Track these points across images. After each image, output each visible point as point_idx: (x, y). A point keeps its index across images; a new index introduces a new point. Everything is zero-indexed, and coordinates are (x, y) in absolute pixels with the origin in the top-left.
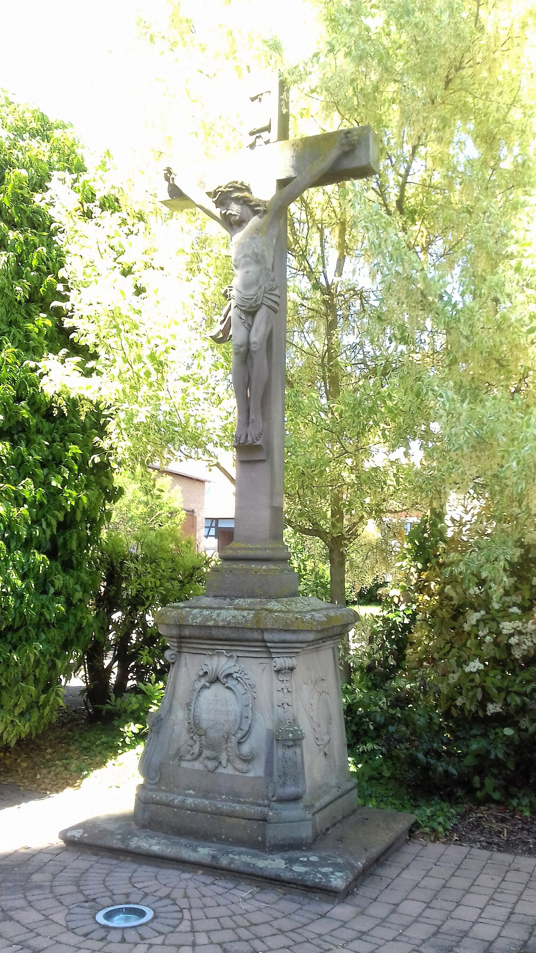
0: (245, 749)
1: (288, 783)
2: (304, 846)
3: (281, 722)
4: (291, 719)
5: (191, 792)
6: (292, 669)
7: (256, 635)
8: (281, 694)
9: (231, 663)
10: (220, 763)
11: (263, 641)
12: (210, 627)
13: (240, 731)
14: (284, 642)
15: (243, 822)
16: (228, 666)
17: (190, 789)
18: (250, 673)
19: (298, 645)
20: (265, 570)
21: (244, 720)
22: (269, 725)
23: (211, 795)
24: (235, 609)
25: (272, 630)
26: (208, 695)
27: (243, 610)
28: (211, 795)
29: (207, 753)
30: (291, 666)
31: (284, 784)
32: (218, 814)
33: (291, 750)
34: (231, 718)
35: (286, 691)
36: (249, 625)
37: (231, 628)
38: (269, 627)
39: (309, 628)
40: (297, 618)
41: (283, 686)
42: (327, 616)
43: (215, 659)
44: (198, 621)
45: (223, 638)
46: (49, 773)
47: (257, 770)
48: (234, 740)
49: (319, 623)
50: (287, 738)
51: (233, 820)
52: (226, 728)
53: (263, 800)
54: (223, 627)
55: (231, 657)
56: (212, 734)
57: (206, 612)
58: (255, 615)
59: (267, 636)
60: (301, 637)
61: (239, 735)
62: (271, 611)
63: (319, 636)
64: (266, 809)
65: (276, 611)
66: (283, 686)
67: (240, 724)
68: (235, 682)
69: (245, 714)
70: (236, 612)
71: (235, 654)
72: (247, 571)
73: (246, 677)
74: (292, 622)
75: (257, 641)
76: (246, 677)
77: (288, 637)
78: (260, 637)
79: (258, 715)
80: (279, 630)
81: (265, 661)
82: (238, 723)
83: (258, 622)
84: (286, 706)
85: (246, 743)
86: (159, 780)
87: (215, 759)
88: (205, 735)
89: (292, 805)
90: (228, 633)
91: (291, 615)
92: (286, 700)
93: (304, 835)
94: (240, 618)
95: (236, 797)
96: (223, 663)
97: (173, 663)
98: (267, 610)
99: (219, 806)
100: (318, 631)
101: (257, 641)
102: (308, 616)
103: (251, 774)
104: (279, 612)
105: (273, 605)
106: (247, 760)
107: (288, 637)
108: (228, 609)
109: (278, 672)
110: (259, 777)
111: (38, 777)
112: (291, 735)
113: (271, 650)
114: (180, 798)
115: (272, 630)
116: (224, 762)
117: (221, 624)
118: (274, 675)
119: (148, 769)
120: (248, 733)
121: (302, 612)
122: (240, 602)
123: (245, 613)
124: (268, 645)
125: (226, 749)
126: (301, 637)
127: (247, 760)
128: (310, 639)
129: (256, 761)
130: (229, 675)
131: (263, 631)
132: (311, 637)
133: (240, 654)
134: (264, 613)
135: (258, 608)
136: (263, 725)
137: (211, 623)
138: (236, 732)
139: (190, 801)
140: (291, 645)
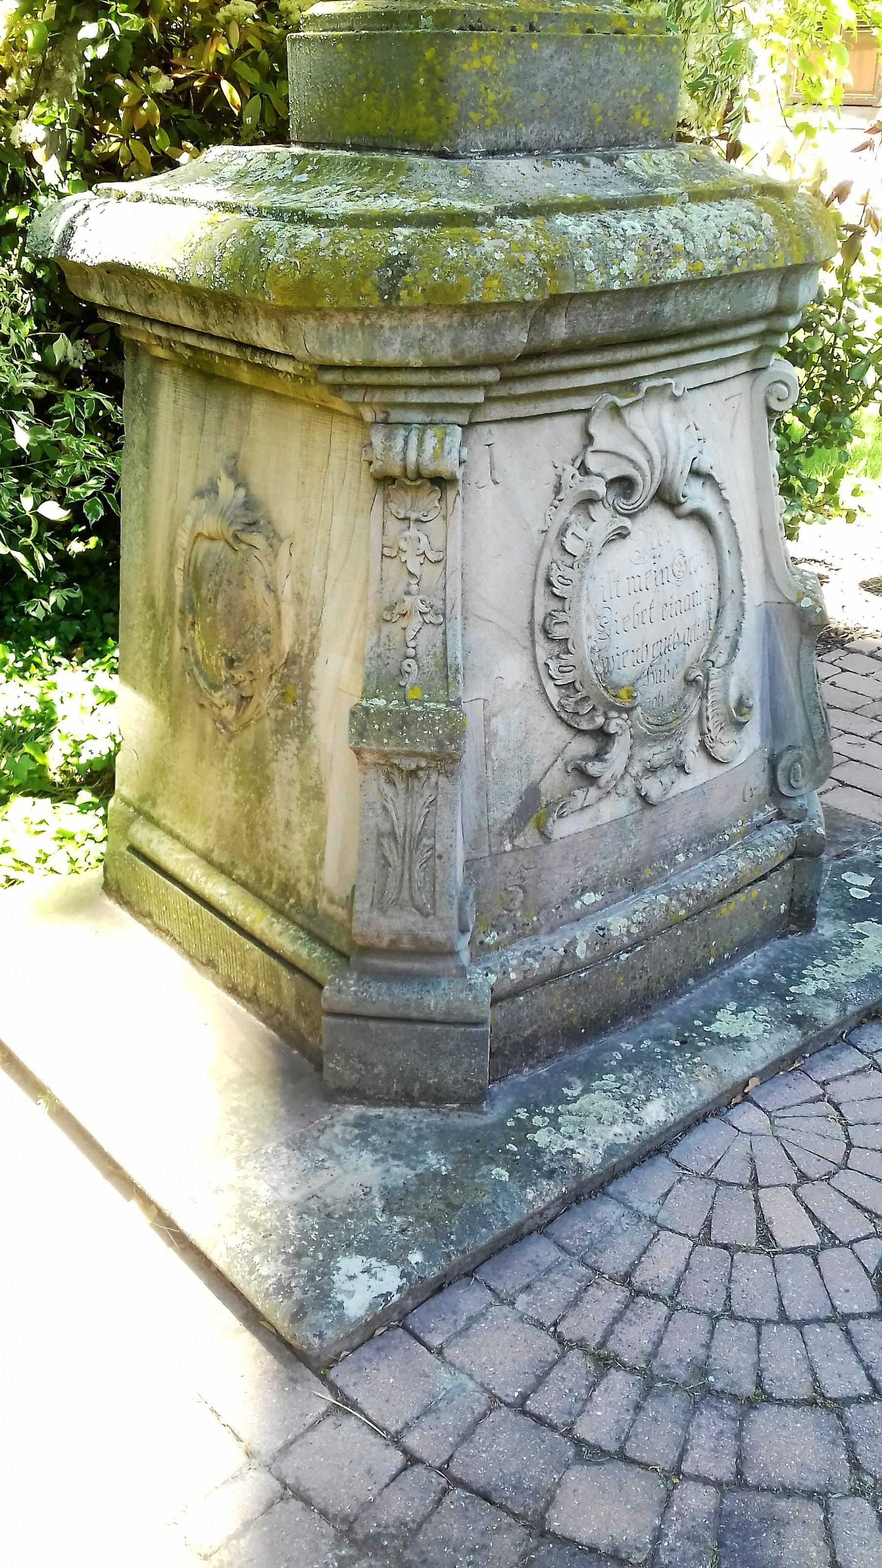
15: (755, 892)
17: (584, 890)
23: (648, 873)
28: (648, 873)
99: (700, 886)
117: (711, 267)
139: (618, 924)
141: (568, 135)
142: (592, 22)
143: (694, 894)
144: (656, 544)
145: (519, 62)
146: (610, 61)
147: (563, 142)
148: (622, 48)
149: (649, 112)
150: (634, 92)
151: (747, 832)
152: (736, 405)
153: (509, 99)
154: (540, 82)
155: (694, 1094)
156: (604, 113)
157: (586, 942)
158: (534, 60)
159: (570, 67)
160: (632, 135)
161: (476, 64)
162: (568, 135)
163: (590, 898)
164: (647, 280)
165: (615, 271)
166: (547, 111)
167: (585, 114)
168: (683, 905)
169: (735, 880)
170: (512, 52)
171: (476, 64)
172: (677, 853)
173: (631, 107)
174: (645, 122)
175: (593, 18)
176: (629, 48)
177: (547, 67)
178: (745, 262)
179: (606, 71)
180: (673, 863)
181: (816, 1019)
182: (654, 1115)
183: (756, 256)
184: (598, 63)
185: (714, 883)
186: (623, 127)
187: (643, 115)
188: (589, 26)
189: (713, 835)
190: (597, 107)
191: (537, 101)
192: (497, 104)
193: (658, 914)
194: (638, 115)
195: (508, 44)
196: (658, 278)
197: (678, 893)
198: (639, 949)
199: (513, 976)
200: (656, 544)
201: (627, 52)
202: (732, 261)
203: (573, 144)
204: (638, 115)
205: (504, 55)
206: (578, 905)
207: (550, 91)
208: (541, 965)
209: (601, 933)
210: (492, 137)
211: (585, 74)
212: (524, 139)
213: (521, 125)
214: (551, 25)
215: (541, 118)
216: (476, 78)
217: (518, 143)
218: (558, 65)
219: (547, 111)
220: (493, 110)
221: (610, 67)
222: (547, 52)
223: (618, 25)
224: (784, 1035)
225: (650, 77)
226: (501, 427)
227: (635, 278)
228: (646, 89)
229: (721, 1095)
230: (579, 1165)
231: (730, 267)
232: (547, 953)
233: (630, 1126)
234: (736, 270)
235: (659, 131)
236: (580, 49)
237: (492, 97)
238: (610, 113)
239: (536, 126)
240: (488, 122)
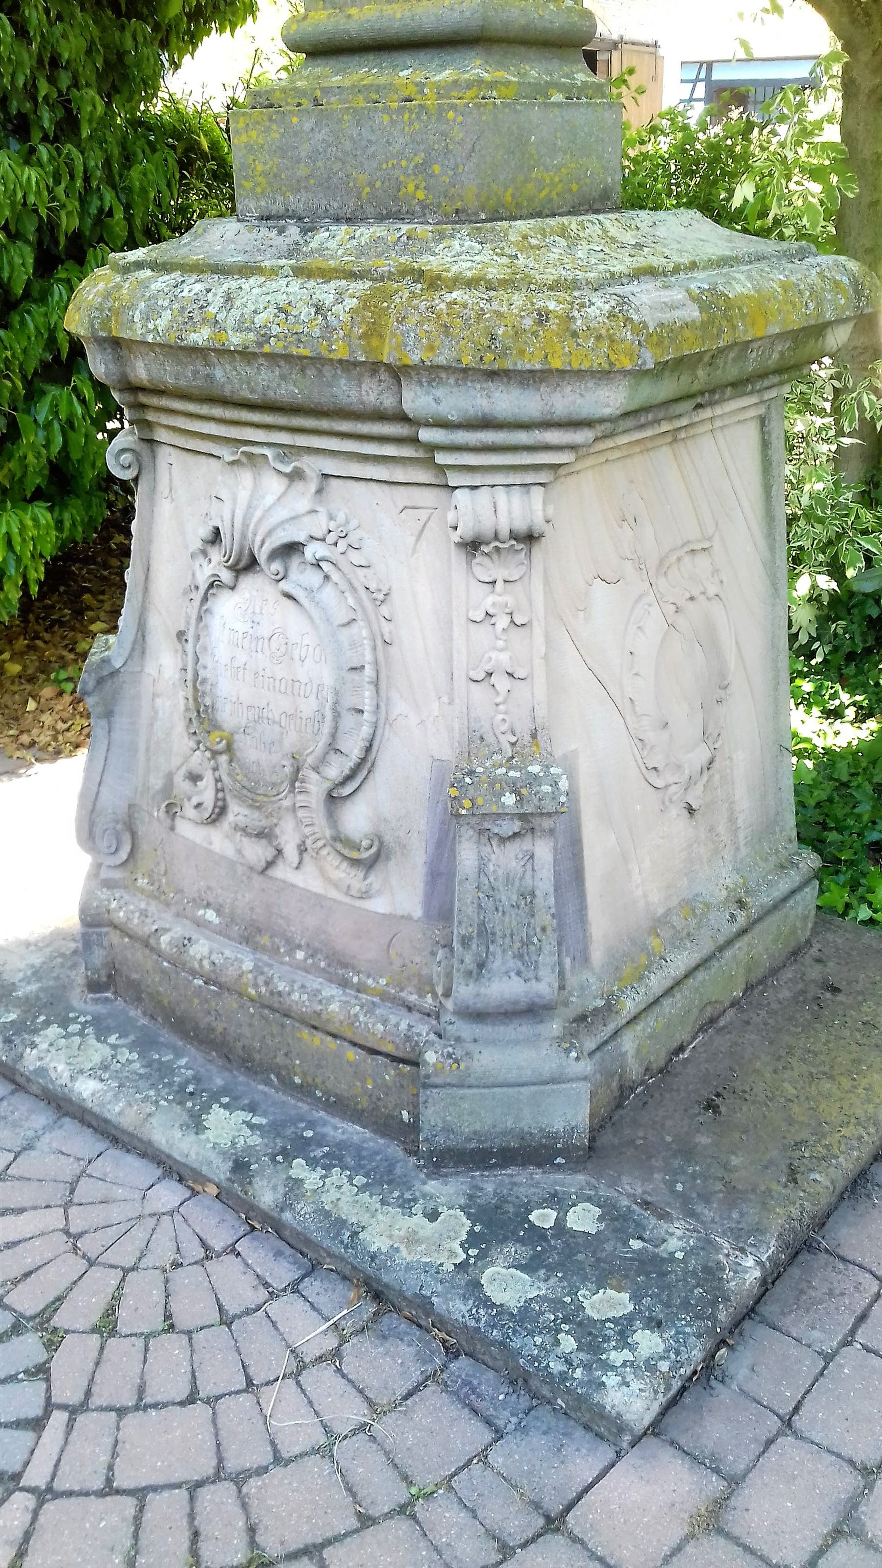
0: (357, 819)
1: (496, 964)
2: (560, 1153)
3: (475, 740)
4: (524, 730)
5: (211, 915)
6: (530, 538)
7: (372, 393)
8: (482, 634)
9: (301, 499)
10: (280, 852)
11: (403, 418)
12: (195, 351)
13: (333, 758)
14: (486, 423)
15: (352, 1054)
16: (282, 514)
17: (208, 905)
18: (370, 546)
19: (553, 437)
20: (442, 91)
21: (348, 721)
22: (443, 746)
23: (265, 940)
24: (298, 272)
25: (431, 373)
26: (228, 608)
27: (326, 275)
28: (265, 940)
29: (237, 812)
30: (521, 526)
31: (481, 966)
32: (275, 1008)
33: (514, 849)
34: (308, 707)
35: (503, 622)
36: (340, 350)
37: (272, 357)
38: (414, 358)
39: (598, 361)
40: (543, 317)
41: (489, 601)
42: (713, 304)
43: (246, 477)
44: (162, 323)
45: (254, 397)
46: (61, 694)
47: (400, 894)
48: (316, 786)
49: (669, 332)
50: (505, 800)
51: (318, 1039)
52: (291, 740)
53: (421, 995)
54: (245, 355)
55: (296, 475)
56: (250, 751)
57: (193, 287)
58: (365, 302)
59: (416, 399)
60: (565, 400)
61: (335, 770)
62: (434, 282)
63: (666, 388)
64: (423, 1030)
65: (458, 282)
66: (489, 601)
67: (334, 735)
68: (313, 578)
69: (349, 701)
70: (295, 286)
71: (312, 465)
72: (375, 94)
73: (355, 557)
74: (518, 333)
75: (380, 416)
76: (355, 557)
77: (505, 401)
78: (388, 402)
79: (400, 707)
80: (464, 373)
81: (427, 497)
82: (326, 729)
83: (374, 331)
84: (502, 683)
85: (360, 797)
86: (132, 854)
87: (264, 835)
88: (229, 748)
89: (523, 1029)
90: (266, 381)
91: (518, 299)
92: (503, 659)
93: (558, 1125)
94: (306, 312)
95: (338, 967)
96: (269, 499)
97: (136, 480)
98: (419, 275)
99: (281, 986)
100: (640, 374)
101: (380, 416)
102: (599, 306)
103: (379, 905)
104: (471, 284)
105: (459, 253)
106: (371, 857)
107: (505, 401)
108: (274, 272)
109: (472, 546)
110: (408, 918)
111: (31, 705)
112: (509, 799)
113: (441, 458)
114: (178, 930)
115: (431, 373)
116: (291, 852)
117: (235, 340)
118: (458, 558)
119: (92, 824)
120: (363, 767)
121: (574, 285)
122: (335, 242)
123: (326, 293)
124: (426, 435)
125: (294, 809)
126: (565, 400)
127: (371, 857)
128: (607, 411)
129: (392, 863)
130: (291, 549)
131: (398, 373)
132: (609, 399)
133: (330, 466)
134: (404, 290)
135: (385, 265)
136: (418, 746)
137: (200, 337)
138: (323, 760)
139: (200, 949)
140: (522, 437)
141: (335, 205)
142: (377, 92)
143: (271, 987)
144: (258, 610)
145: (282, 135)
146: (373, 131)
147: (331, 211)
148: (386, 118)
149: (423, 184)
150: (404, 163)
151: (385, 997)
152: (424, 518)
153: (275, 170)
154: (303, 154)
155: (117, 1109)
156: (371, 185)
157: (172, 938)
158: (296, 134)
159: (331, 139)
160: (405, 209)
161: (244, 138)
162: (335, 205)
163: (211, 915)
164: (172, 340)
165: (151, 326)
166: (312, 181)
167: (351, 184)
168: (256, 986)
169: (319, 1014)
170: (274, 127)
171: (244, 138)
172: (299, 947)
173: (402, 178)
174: (420, 195)
175: (378, 89)
176: (394, 117)
177: (310, 139)
178: (281, 344)
179: (369, 141)
180: (291, 952)
181: (250, 1183)
182: (84, 1087)
183: (300, 341)
184: (360, 134)
185: (295, 996)
186: (395, 199)
187: (417, 187)
188: (375, 97)
189: (345, 966)
190: (363, 178)
191: (302, 171)
192: (264, 174)
193: (232, 972)
194: (411, 188)
195: (270, 120)
196: (182, 340)
197: (262, 973)
198: (212, 987)
199: (121, 914)
200: (258, 610)
201: (392, 122)
202: (266, 338)
203: (342, 215)
204: (411, 188)
205: (268, 130)
206: (201, 912)
207: (314, 162)
208: (138, 925)
209: (186, 942)
210: (263, 203)
211: (348, 146)
212: (293, 207)
213: (288, 194)
214: (333, 99)
215: (306, 188)
216: (244, 151)
217: (287, 210)
218: (319, 137)
219: (312, 181)
220: (260, 179)
221: (373, 138)
222: (307, 126)
223: (406, 93)
224: (217, 1160)
225: (422, 147)
226: (178, 452)
227: (164, 335)
228: (419, 159)
229: (130, 1134)
230: (22, 1056)
231: (260, 344)
232: (149, 920)
233: (66, 1074)
234: (267, 349)
235: (439, 205)
236: (340, 121)
237: (260, 168)
238: (378, 184)
239: (304, 196)
240: (259, 190)
